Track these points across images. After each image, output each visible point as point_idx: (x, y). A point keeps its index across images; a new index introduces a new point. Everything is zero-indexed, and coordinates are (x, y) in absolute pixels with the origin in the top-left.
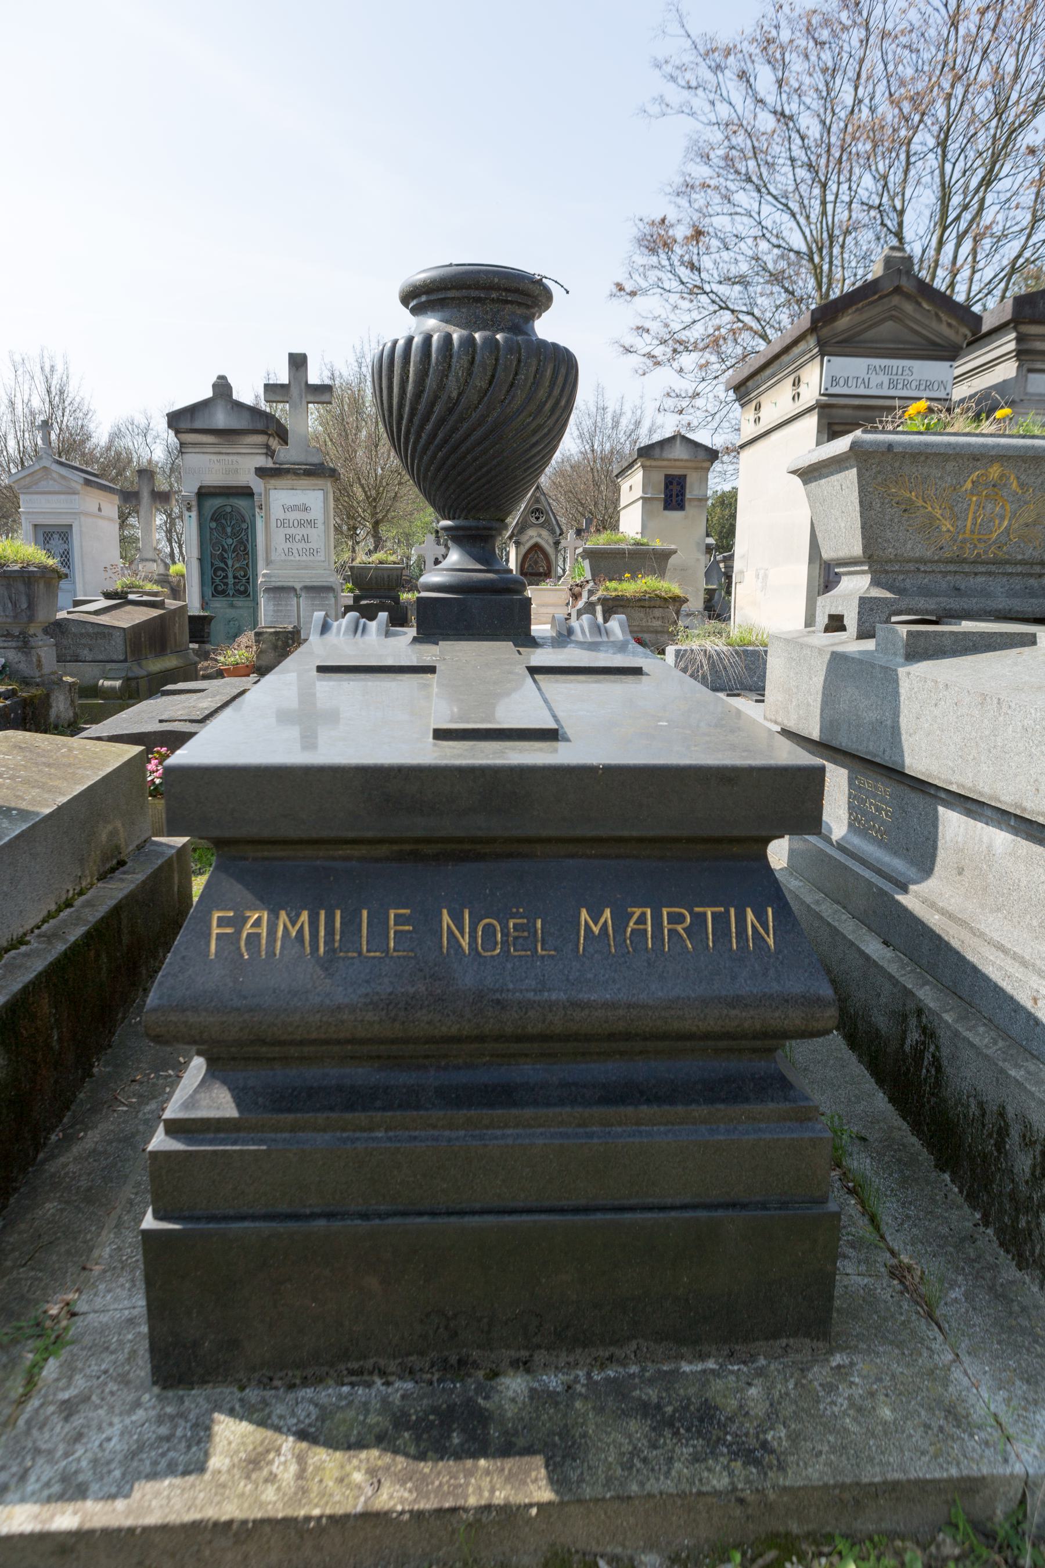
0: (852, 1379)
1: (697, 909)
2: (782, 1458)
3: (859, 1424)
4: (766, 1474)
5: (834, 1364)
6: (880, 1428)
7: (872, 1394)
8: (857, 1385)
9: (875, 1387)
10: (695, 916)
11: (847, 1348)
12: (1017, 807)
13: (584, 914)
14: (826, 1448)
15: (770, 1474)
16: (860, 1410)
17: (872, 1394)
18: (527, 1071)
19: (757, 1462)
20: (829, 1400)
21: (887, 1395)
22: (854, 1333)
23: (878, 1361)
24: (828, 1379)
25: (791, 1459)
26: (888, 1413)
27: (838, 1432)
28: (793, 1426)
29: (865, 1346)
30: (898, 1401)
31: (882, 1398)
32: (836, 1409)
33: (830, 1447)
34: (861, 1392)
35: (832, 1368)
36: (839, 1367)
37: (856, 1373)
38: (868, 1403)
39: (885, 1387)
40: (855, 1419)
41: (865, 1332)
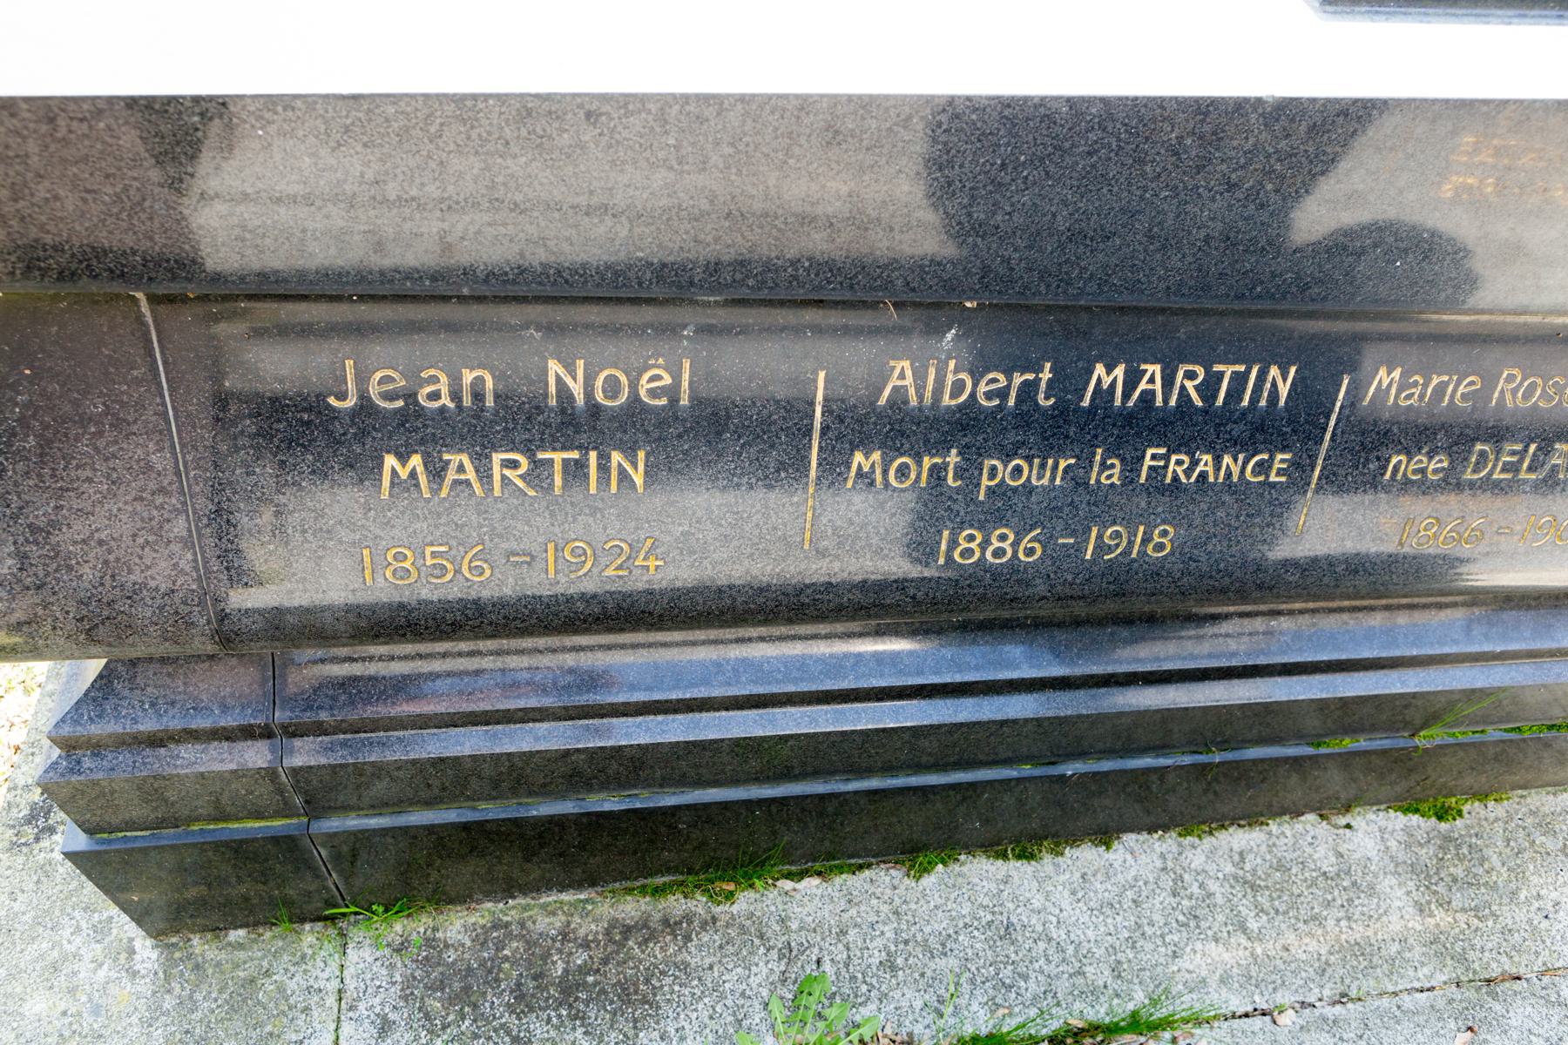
0: (105, 967)
1: (541, 455)
2: (24, 849)
3: (36, 960)
4: (14, 827)
5: (138, 944)
6: (18, 990)
7: (72, 991)
8: (95, 971)
9: (84, 999)
10: (536, 464)
11: (168, 977)
12: (495, 735)
13: (554, 367)
14: (17, 906)
15: (11, 832)
16: (55, 968)
17: (72, 991)
18: (369, 374)
19: (31, 819)
20: (84, 925)
21: (64, 1013)
22: (198, 996)
23: (134, 1019)
24: (115, 931)
25: (21, 859)
26: (37, 1009)
27: (32, 928)
28: (61, 870)
29: (166, 1006)
30: (50, 1029)
31: (62, 1006)
32: (67, 933)
33: (16, 914)
34: (81, 976)
35: (131, 940)
36: (132, 952)
37: (113, 974)
38: (61, 981)
39: (79, 1014)
40: (42, 957)
41: (198, 1015)
